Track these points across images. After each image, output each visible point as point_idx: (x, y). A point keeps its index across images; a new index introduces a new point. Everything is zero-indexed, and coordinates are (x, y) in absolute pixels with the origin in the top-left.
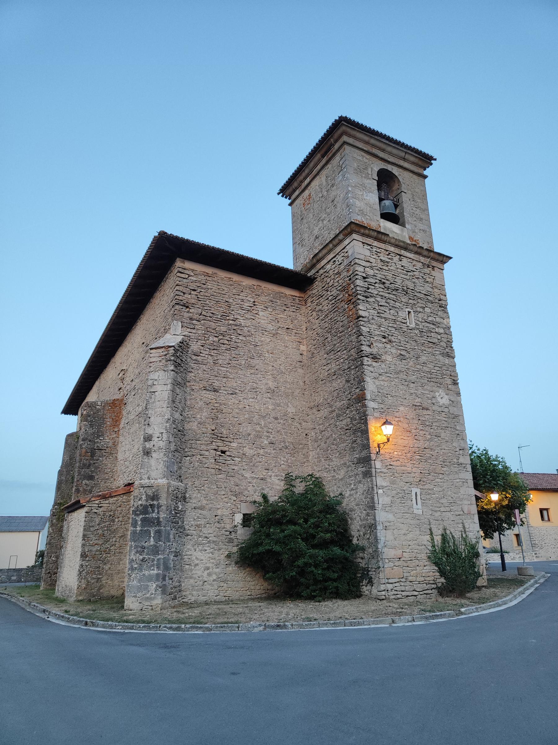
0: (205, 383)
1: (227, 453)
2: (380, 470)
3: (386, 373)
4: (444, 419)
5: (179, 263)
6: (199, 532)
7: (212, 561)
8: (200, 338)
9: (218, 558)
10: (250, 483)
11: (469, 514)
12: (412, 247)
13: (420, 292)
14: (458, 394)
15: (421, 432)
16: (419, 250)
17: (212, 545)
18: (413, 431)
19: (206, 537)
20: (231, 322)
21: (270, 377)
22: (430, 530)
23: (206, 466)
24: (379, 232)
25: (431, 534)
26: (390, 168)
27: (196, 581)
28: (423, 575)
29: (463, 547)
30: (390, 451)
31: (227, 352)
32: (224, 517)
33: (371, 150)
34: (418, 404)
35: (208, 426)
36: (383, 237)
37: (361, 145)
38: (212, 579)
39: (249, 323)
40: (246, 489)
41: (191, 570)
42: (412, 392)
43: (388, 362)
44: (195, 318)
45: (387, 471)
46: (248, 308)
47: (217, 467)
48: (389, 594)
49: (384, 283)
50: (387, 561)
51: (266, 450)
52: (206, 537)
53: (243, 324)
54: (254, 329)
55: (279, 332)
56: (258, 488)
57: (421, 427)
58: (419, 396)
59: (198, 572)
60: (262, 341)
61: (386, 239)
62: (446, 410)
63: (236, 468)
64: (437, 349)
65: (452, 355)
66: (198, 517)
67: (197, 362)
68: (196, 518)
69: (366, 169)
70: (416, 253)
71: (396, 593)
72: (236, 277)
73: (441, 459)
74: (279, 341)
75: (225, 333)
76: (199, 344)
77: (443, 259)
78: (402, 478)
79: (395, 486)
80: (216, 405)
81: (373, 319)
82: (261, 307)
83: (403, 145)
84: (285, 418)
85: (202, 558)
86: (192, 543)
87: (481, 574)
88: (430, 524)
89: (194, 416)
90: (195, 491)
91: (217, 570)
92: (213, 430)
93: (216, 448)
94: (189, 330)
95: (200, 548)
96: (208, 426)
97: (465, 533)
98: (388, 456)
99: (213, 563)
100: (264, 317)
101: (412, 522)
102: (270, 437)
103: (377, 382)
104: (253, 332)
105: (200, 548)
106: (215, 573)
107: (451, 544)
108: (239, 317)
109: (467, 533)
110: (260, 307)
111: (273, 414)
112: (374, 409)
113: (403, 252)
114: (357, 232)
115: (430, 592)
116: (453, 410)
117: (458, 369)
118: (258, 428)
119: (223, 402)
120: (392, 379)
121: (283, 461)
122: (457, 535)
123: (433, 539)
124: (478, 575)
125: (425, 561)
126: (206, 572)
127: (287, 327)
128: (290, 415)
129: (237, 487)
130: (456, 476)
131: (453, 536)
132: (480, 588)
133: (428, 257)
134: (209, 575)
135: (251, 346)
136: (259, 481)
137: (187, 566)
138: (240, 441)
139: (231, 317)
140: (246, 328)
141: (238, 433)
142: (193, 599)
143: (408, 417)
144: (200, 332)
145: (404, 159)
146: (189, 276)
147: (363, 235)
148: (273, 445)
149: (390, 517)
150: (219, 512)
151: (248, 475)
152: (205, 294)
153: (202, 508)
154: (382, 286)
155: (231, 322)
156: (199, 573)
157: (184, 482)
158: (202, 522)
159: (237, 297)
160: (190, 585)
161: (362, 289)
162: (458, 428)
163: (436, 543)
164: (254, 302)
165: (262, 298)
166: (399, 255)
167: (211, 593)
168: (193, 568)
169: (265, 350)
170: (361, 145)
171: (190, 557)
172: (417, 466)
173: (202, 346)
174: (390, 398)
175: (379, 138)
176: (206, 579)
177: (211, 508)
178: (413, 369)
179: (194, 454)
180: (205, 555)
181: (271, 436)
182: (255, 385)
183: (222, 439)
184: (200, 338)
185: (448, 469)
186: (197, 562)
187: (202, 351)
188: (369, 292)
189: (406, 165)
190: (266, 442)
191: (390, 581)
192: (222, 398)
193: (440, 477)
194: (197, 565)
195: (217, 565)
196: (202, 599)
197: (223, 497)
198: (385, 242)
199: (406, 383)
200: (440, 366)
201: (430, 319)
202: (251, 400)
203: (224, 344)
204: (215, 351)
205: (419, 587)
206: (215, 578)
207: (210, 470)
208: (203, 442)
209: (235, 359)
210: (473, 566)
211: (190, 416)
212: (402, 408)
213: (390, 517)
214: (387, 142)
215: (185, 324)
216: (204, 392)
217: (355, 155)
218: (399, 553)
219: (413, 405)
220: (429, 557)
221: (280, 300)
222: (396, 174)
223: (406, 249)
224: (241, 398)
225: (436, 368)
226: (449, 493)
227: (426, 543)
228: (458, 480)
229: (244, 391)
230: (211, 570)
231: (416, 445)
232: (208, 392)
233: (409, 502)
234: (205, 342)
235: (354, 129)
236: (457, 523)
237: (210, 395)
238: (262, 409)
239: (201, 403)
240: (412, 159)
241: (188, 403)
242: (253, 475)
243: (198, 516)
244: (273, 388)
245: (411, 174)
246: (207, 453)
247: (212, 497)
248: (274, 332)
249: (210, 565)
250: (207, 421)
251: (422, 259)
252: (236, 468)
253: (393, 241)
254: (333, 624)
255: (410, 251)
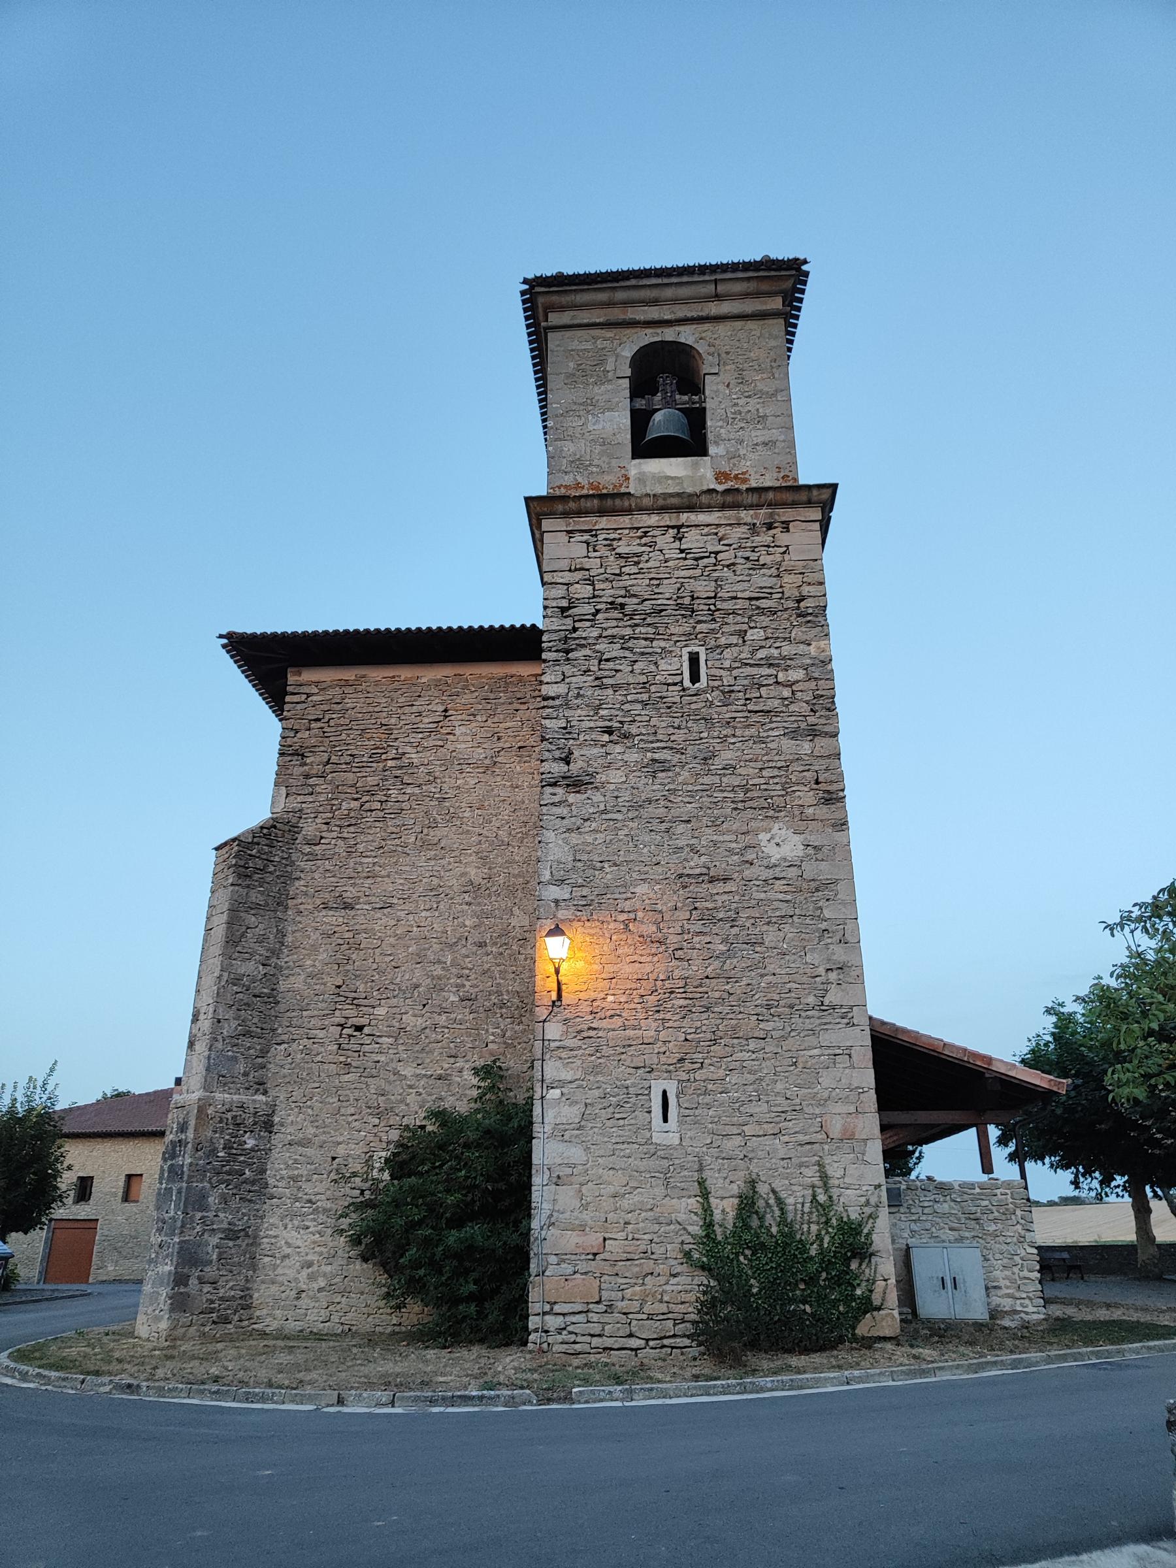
0: (327, 895)
1: (366, 1030)
2: (557, 1044)
3: (602, 812)
4: (781, 896)
5: (291, 679)
6: (295, 1191)
7: (317, 1249)
8: (321, 809)
9: (331, 1244)
10: (410, 1087)
11: (848, 1136)
12: (704, 499)
13: (736, 598)
14: (842, 825)
15: (696, 939)
16: (729, 499)
17: (322, 1218)
18: (673, 939)
19: (310, 1201)
20: (390, 763)
21: (473, 858)
22: (701, 1183)
23: (319, 1058)
24: (602, 497)
25: (705, 1194)
26: (669, 334)
27: (283, 1288)
28: (666, 1298)
29: (814, 1228)
30: (593, 995)
31: (377, 824)
32: (350, 1160)
33: (622, 317)
34: (698, 871)
35: (327, 979)
36: (618, 502)
37: (598, 316)
38: (316, 1286)
39: (429, 756)
40: (402, 1101)
41: (275, 1267)
42: (680, 843)
43: (612, 787)
44: (314, 772)
45: (580, 1043)
46: (431, 726)
47: (342, 1059)
48: (550, 1340)
49: (622, 606)
50: (553, 1259)
51: (453, 1016)
52: (310, 1201)
53: (415, 761)
54: (441, 766)
55: (499, 759)
56: (429, 1098)
57: (698, 927)
58: (703, 851)
59: (288, 1271)
60: (458, 787)
61: (626, 504)
62: (793, 873)
63: (382, 1058)
64: (773, 725)
65: (827, 729)
66: (296, 1162)
67: (312, 857)
68: (290, 1162)
69: (602, 362)
70: (723, 507)
71: (572, 1338)
72: (405, 673)
73: (759, 999)
74: (499, 779)
75: (376, 788)
76: (318, 820)
77: (824, 498)
78: (623, 1057)
79: (600, 1078)
80: (347, 935)
81: (578, 696)
82: (459, 717)
83: (703, 269)
84: (503, 940)
85: (299, 1243)
86: (279, 1212)
87: (876, 1301)
88: (701, 1170)
89: (300, 963)
90: (292, 1109)
91: (329, 1268)
92: (339, 987)
93: (343, 1021)
94: (300, 799)
95: (296, 1223)
96: (327, 979)
97: (826, 1191)
98: (585, 1008)
99: (321, 1254)
100: (465, 738)
101: (643, 1165)
102: (464, 986)
103: (574, 838)
104: (437, 774)
105: (296, 1223)
106: (325, 1275)
107: (769, 1219)
108: (408, 749)
109: (835, 1192)
110: (456, 719)
111: (475, 937)
112: (557, 902)
113: (684, 517)
114: (551, 514)
115: (679, 1342)
116: (824, 870)
117: (847, 764)
118: (438, 971)
119: (363, 927)
120: (619, 825)
121: (493, 1034)
122: (796, 1198)
123: (707, 1210)
124: (867, 1306)
125: (674, 1262)
126: (305, 1272)
127: (519, 744)
128: (517, 933)
129: (381, 1099)
130: (812, 1041)
131: (780, 1202)
132: (868, 1343)
133: (759, 506)
134: (311, 1278)
135: (432, 803)
136: (434, 1082)
137: (267, 1259)
138: (394, 1001)
139: (392, 753)
140: (422, 768)
141: (391, 987)
142: (275, 1325)
143: (659, 907)
144: (322, 798)
145: (718, 297)
146: (308, 695)
147: (566, 514)
148: (469, 1003)
149: (576, 1153)
150: (341, 1151)
151: (408, 1071)
152: (338, 722)
153: (305, 1143)
154: (616, 614)
155: (390, 763)
156: (291, 1274)
157: (272, 1093)
158: (303, 1171)
159: (407, 710)
160: (269, 1296)
161: (554, 637)
162: (827, 913)
163: (717, 1216)
164: (446, 711)
165: (467, 698)
166: (673, 527)
167: (314, 1315)
168: (278, 1262)
169: (463, 805)
170: (585, 317)
171: (273, 1240)
172: (675, 1024)
173: (327, 824)
174: (608, 870)
175: (633, 282)
176: (304, 1287)
177: (325, 1142)
178: (690, 788)
179: (295, 1037)
180: (305, 1237)
181: (467, 984)
182: (436, 881)
183: (354, 1003)
184: (321, 809)
185: (780, 1025)
186: (288, 1251)
187: (324, 834)
188: (575, 639)
189: (726, 308)
190: (453, 998)
191: (557, 1309)
192: (361, 919)
193: (751, 1047)
194: (287, 1256)
195: (331, 1258)
196: (293, 1326)
197: (351, 1119)
198: (629, 511)
199: (664, 826)
200: (779, 764)
201: (761, 654)
202: (424, 914)
203: (372, 811)
204: (352, 829)
205: (650, 1329)
206: (323, 1285)
207: (326, 1066)
208: (316, 1013)
209: (394, 836)
210: (845, 1280)
211: (291, 964)
212: (641, 889)
213: (576, 1153)
214: (659, 281)
215: (294, 790)
216: (324, 913)
217: (575, 345)
218: (593, 1240)
219: (681, 876)
220: (688, 1255)
221: (505, 692)
222: (690, 341)
223: (691, 508)
224: (402, 914)
225: (765, 773)
226: (779, 1086)
227: (682, 1217)
228: (816, 1052)
229: (409, 897)
230: (315, 1268)
231: (677, 974)
232: (331, 913)
233: (641, 1116)
234: (331, 815)
235: (566, 291)
236: (801, 1165)
237: (333, 918)
238: (449, 929)
239: (315, 936)
240: (738, 287)
241: (289, 939)
242: (418, 1072)
243: (296, 1160)
244: (478, 880)
245: (738, 324)
246: (321, 1034)
247: (328, 1121)
248: (487, 762)
249: (315, 1258)
250: (327, 969)
251: (746, 516)
252: (382, 1058)
253: (646, 502)
254: (214, 1393)
255: (708, 508)
